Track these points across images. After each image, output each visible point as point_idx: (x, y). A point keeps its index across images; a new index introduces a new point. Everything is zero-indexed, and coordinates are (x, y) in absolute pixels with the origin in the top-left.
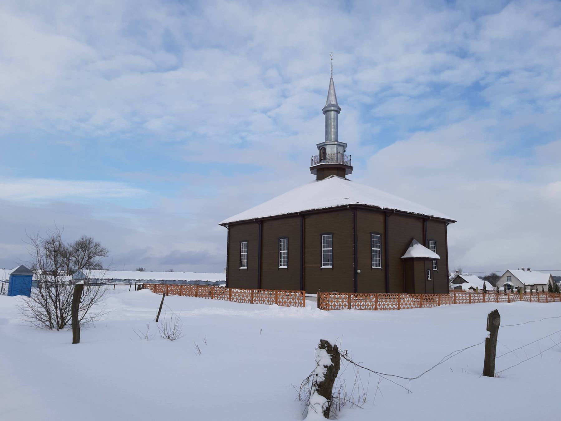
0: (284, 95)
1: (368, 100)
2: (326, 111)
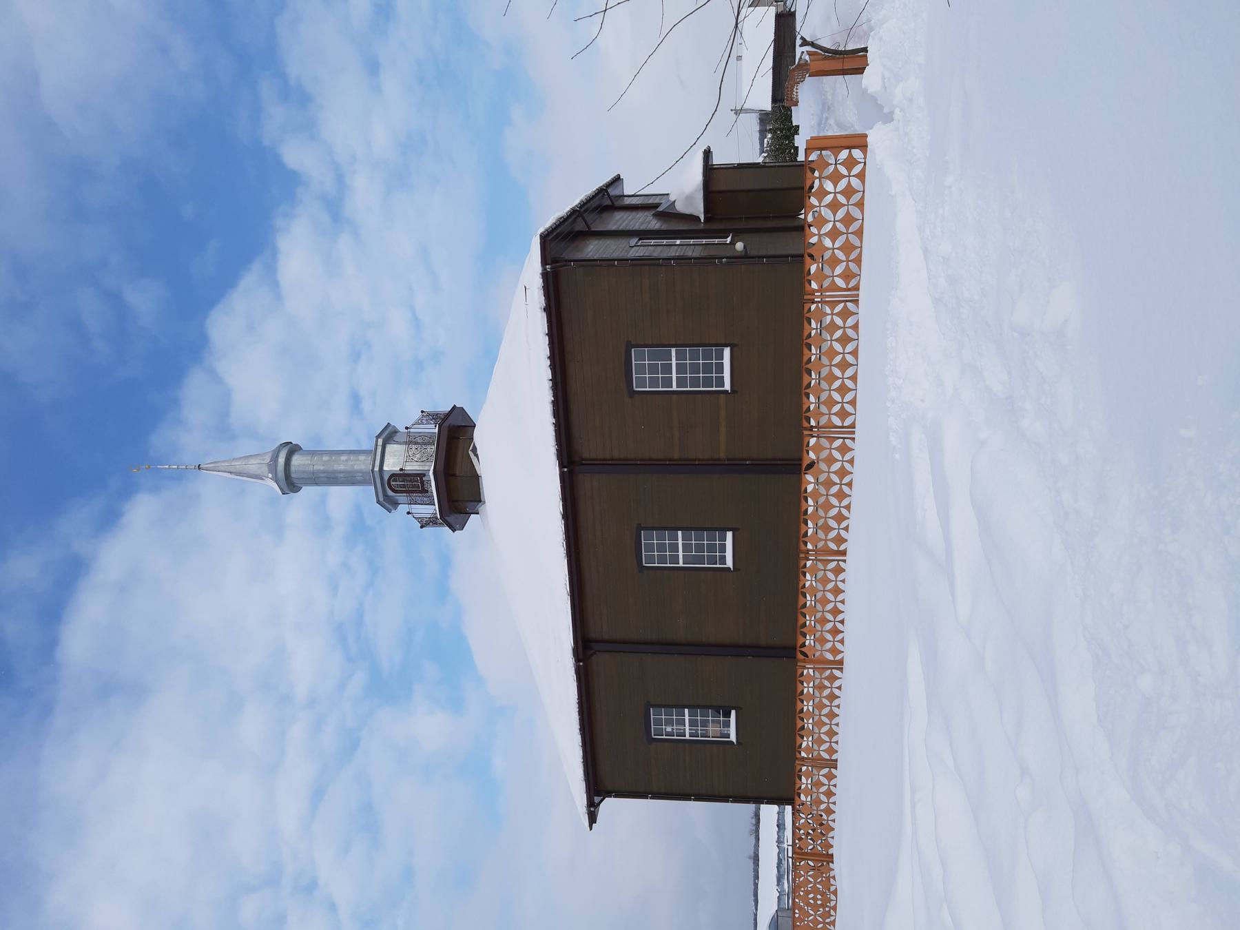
0: (309, 887)
1: (360, 678)
2: (290, 484)
